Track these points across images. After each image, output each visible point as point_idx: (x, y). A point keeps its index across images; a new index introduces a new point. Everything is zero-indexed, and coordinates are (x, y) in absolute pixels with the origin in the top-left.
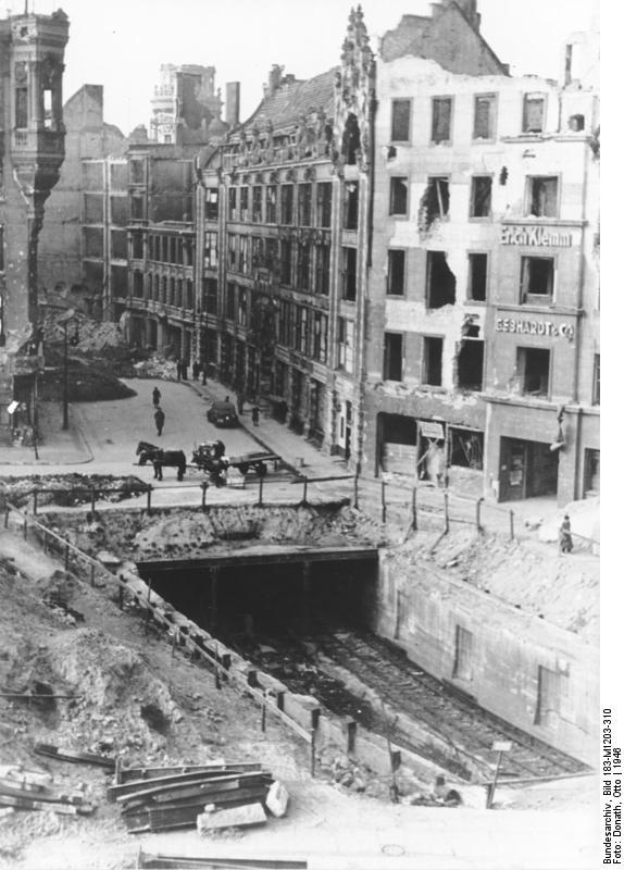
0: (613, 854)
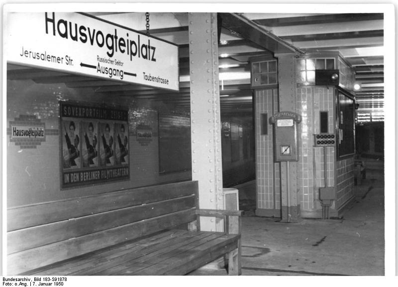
0: (7, 282)
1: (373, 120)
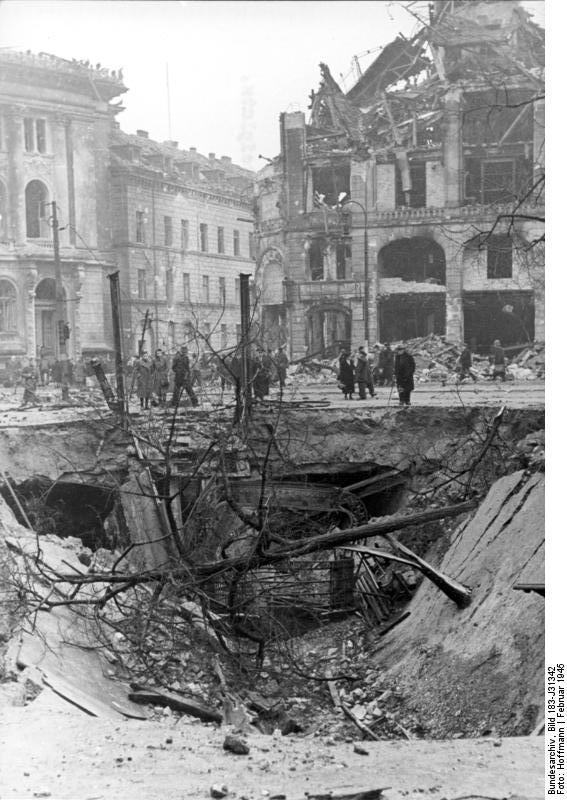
0: (557, 786)
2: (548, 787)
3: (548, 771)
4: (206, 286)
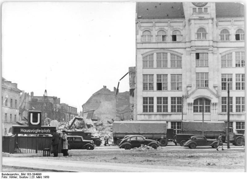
0: (4, 176)
1: (204, 122)
2: (4, 173)
3: (9, 173)
4: (6, 117)
